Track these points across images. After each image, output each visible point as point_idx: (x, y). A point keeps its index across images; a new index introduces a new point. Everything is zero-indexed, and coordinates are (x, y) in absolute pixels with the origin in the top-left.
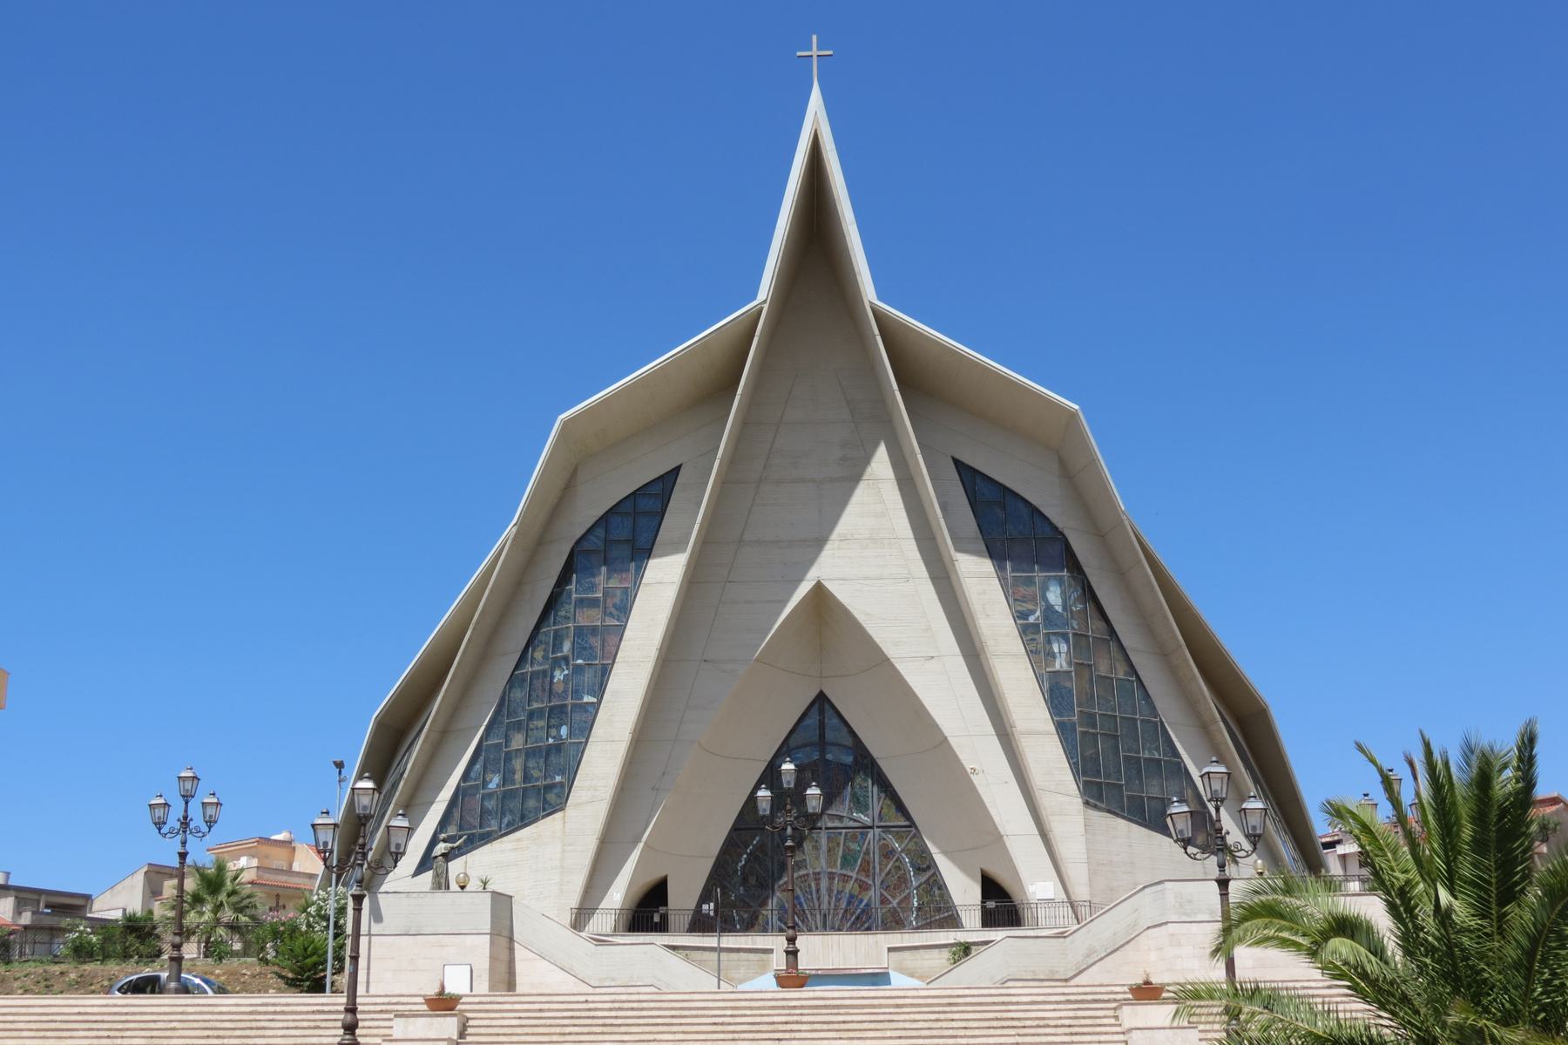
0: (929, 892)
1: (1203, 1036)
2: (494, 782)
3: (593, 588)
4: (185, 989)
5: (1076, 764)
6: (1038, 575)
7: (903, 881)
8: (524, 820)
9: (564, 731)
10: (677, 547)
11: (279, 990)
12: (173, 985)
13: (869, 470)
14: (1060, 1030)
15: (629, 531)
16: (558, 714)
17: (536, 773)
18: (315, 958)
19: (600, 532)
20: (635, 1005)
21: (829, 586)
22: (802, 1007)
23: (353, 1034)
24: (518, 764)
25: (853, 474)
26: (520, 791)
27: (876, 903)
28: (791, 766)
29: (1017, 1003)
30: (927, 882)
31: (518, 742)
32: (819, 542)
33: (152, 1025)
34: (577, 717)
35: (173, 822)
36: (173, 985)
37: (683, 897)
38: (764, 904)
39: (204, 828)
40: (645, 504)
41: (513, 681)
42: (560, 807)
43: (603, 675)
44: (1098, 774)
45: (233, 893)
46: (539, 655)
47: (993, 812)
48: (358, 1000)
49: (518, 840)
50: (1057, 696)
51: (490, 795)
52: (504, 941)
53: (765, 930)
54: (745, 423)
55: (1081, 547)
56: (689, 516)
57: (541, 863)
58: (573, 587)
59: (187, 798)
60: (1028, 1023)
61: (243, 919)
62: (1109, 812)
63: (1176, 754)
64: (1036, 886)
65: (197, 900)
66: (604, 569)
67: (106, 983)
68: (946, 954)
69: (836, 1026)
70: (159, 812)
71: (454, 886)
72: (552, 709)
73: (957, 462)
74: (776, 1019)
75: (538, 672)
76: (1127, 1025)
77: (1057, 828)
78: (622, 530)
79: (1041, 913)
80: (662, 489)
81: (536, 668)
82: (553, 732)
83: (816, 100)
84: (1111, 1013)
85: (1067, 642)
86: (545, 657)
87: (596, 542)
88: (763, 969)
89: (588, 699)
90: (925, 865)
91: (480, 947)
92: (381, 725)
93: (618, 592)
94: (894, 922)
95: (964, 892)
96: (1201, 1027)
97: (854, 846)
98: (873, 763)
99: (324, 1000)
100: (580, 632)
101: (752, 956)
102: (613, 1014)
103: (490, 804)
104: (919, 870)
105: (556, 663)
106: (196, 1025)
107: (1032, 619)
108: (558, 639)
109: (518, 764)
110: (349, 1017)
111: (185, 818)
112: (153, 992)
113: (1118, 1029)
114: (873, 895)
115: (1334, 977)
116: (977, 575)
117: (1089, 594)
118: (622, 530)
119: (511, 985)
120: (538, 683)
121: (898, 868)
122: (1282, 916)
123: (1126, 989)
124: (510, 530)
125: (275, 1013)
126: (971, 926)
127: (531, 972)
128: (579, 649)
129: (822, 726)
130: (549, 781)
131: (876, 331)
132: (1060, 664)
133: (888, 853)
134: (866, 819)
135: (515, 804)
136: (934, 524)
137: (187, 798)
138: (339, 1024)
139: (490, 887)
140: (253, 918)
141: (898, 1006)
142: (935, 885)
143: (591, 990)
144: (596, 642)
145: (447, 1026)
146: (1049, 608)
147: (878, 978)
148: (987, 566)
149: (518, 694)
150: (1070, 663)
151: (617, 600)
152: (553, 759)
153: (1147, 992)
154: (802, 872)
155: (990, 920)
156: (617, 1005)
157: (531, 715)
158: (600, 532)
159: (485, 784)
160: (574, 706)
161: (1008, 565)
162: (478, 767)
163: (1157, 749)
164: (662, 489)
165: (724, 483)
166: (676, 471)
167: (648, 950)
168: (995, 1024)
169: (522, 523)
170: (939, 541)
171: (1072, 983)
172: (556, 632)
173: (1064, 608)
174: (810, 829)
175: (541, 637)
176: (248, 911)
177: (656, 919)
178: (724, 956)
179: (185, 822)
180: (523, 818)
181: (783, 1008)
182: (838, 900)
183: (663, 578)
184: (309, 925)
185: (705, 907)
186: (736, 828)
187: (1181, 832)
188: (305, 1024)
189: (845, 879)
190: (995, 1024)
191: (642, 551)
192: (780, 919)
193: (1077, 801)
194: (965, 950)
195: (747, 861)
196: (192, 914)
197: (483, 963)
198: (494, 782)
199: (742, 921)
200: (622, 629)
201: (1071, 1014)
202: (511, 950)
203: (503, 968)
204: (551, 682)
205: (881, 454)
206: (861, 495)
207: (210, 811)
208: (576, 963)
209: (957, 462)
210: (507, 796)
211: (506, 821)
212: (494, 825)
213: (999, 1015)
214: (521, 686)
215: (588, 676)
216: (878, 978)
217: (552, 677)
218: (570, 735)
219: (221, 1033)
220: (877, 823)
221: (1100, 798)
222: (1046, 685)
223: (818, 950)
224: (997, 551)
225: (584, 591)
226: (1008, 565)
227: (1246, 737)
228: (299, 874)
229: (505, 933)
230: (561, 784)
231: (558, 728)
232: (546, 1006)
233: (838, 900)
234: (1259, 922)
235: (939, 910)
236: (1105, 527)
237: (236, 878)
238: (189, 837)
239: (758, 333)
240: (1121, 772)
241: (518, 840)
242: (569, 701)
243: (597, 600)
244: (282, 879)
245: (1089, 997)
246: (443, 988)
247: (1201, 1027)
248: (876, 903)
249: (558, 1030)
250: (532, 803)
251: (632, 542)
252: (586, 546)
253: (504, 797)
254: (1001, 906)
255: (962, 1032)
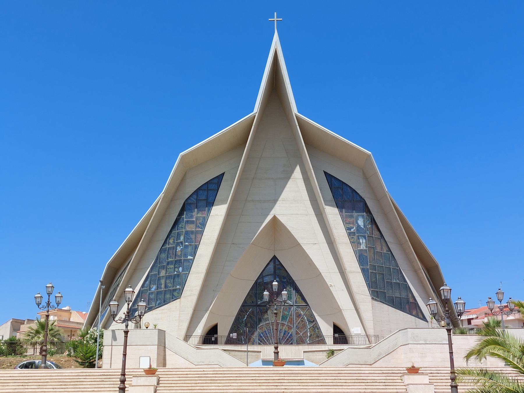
0: (314, 330)
1: (435, 387)
2: (154, 288)
3: (192, 217)
4: (46, 367)
5: (369, 284)
6: (355, 214)
7: (304, 326)
8: (165, 302)
9: (181, 269)
10: (223, 202)
11: (76, 367)
12: (43, 365)
13: (293, 175)
14: (381, 384)
15: (205, 196)
16: (178, 263)
17: (169, 285)
18: (90, 354)
19: (195, 196)
20: (222, 372)
21: (279, 217)
22: (284, 374)
23: (124, 384)
24: (163, 281)
25: (287, 176)
26: (165, 291)
27: (294, 334)
28: (276, 283)
29: (364, 373)
30: (313, 326)
31: (163, 273)
32: (275, 201)
33: (39, 381)
34: (185, 264)
35: (44, 303)
36: (43, 365)
37: (223, 332)
38: (253, 334)
39: (56, 306)
40: (211, 187)
41: (161, 251)
42: (178, 297)
43: (195, 249)
44: (377, 287)
45: (52, 330)
46: (171, 241)
47: (338, 301)
48: (126, 371)
49: (162, 310)
50: (361, 258)
51: (152, 293)
52: (162, 348)
53: (253, 344)
54: (248, 157)
55: (370, 204)
56: (227, 191)
57: (172, 317)
58: (184, 216)
59: (49, 294)
60: (369, 381)
61: (56, 340)
62: (381, 302)
63: (405, 281)
64: (354, 329)
65: (37, 332)
66: (196, 210)
67: (9, 364)
68: (325, 354)
69: (297, 381)
70: (38, 300)
71: (143, 327)
72: (176, 261)
73: (325, 173)
74: (274, 378)
75: (171, 247)
76: (406, 383)
77: (362, 307)
78: (203, 196)
79: (355, 339)
80: (218, 180)
81: (170, 246)
82: (177, 270)
83: (276, 43)
84: (399, 378)
85: (365, 239)
86: (174, 242)
87: (193, 200)
88: (257, 358)
89: (189, 257)
90: (313, 320)
91: (154, 350)
92: (109, 267)
93: (201, 218)
94: (301, 341)
95: (327, 331)
96: (435, 384)
97: (286, 313)
98: (293, 282)
99: (96, 371)
100: (187, 233)
101: (253, 354)
102: (214, 376)
103: (152, 296)
104: (310, 322)
105: (178, 244)
106: (56, 380)
107: (352, 230)
108: (179, 235)
109: (163, 281)
110: (123, 377)
111: (49, 302)
112: (32, 368)
113: (403, 384)
114: (293, 331)
115: (514, 368)
116: (333, 214)
117: (373, 221)
118: (203, 196)
119: (164, 365)
120: (171, 252)
121: (303, 321)
122: (499, 345)
123: (405, 369)
124: (161, 195)
125: (86, 376)
126: (330, 344)
127: (172, 360)
128: (187, 239)
129: (275, 267)
130: (174, 288)
131: (297, 125)
132: (363, 247)
133: (299, 315)
134: (291, 303)
135: (161, 296)
136: (317, 196)
137: (49, 294)
138: (119, 380)
139: (157, 327)
140: (58, 339)
141: (319, 374)
142: (316, 327)
143: (194, 367)
144: (193, 236)
145: (153, 380)
146: (359, 226)
147: (300, 363)
148: (336, 210)
149: (163, 256)
150: (366, 247)
151: (201, 221)
152: (176, 279)
153: (413, 370)
154: (267, 322)
155: (336, 341)
156: (215, 372)
157: (168, 263)
158: (195, 196)
159: (150, 289)
160: (184, 260)
161: (344, 210)
162: (147, 282)
163: (398, 279)
164: (218, 180)
165: (240, 179)
166: (223, 174)
167: (215, 353)
168: (356, 381)
169: (166, 193)
170: (318, 201)
171: (373, 366)
172: (178, 233)
173: (364, 226)
174: (268, 308)
175: (172, 234)
176: (57, 337)
177: (213, 339)
178: (249, 353)
179: (48, 304)
180: (164, 301)
181: (277, 374)
182: (280, 333)
183: (218, 213)
184: (87, 341)
185: (231, 335)
186: (243, 306)
187: (433, 311)
188: (98, 380)
189: (283, 325)
190: (356, 381)
191: (210, 204)
192: (259, 340)
193: (369, 298)
194: (332, 353)
195: (247, 318)
196: (36, 338)
197: (154, 356)
198: (154, 288)
199: (245, 340)
200: (202, 233)
201: (385, 378)
202: (165, 351)
203: (162, 358)
204: (176, 251)
205: (298, 169)
206: (290, 184)
207: (58, 299)
208: (188, 357)
209: (325, 173)
210: (158, 293)
211: (158, 302)
212: (153, 304)
213: (358, 378)
214: (165, 252)
215: (190, 249)
216: (300, 363)
217: (176, 249)
218: (183, 271)
219: (66, 383)
220: (295, 304)
221: (378, 297)
222: (357, 256)
223: (287, 352)
224: (340, 206)
225: (189, 218)
226: (344, 210)
227: (429, 275)
228: (73, 322)
229: (163, 345)
230: (179, 289)
231: (178, 268)
232: (189, 373)
233: (280, 333)
234: (493, 346)
235: (318, 337)
236: (379, 199)
237: (53, 324)
238: (50, 309)
239: (254, 124)
240: (387, 288)
241: (162, 310)
242: (183, 258)
243: (193, 221)
244: (66, 325)
245: (391, 372)
246: (150, 366)
247: (435, 384)
248: (294, 334)
249: (194, 382)
250: (168, 296)
251: (206, 200)
252: (189, 201)
253: (157, 294)
254: (341, 336)
255: (345, 384)
